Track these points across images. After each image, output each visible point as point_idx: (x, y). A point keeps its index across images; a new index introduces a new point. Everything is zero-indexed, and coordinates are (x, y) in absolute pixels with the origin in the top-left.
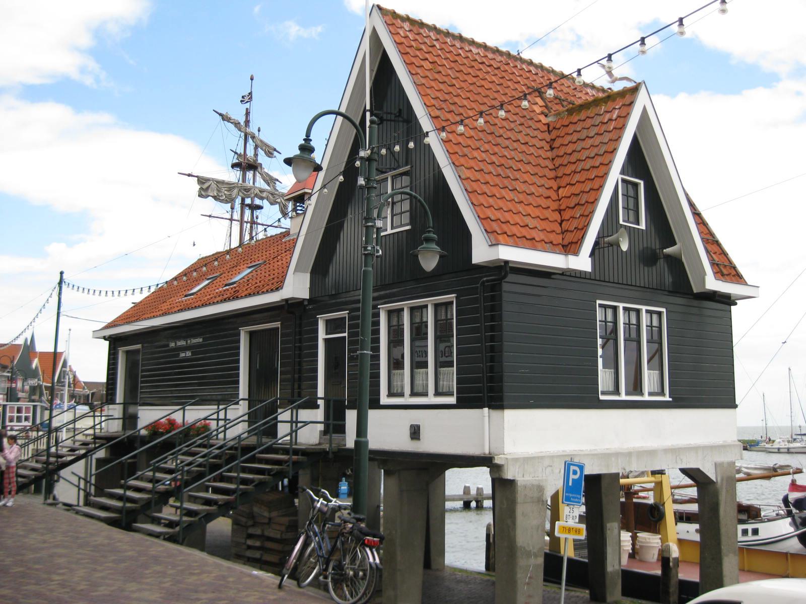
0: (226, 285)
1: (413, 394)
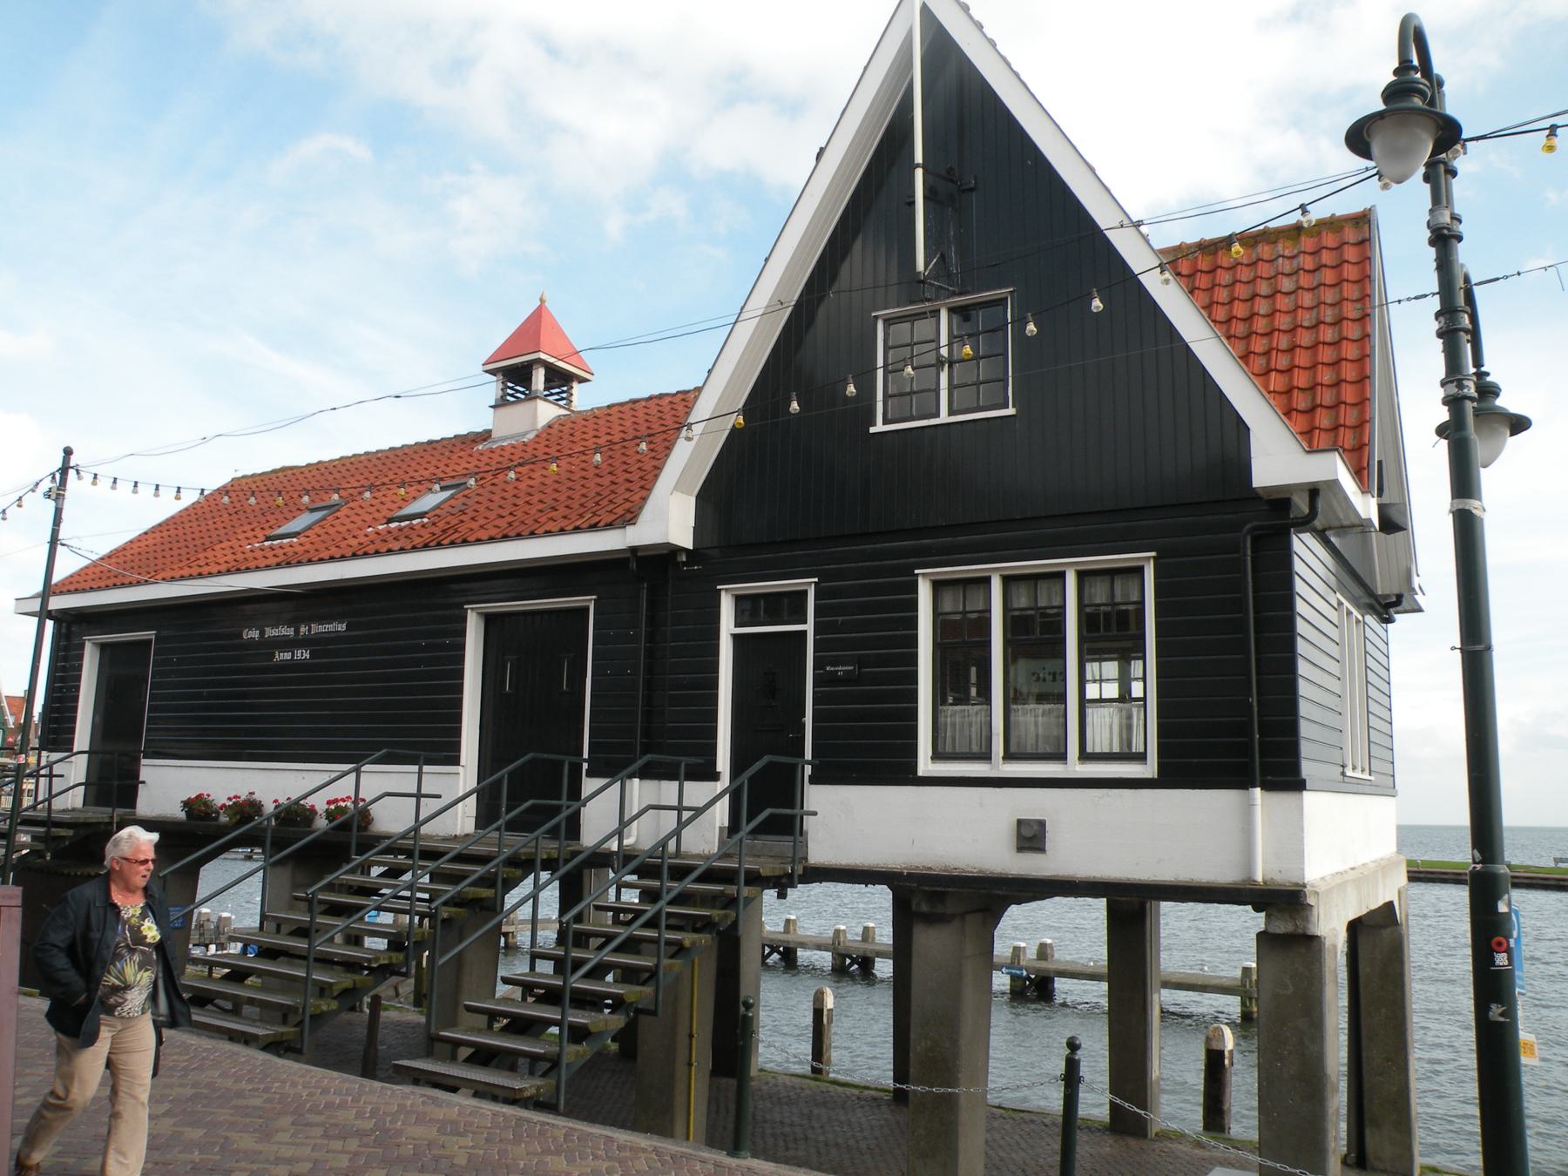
0: (268, 539)
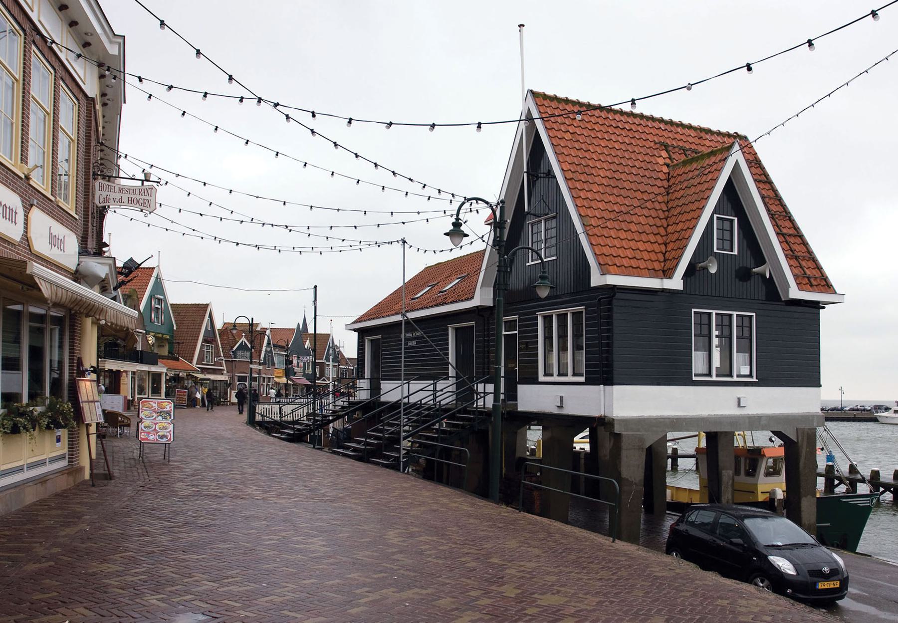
0: (440, 292)
1: (560, 375)
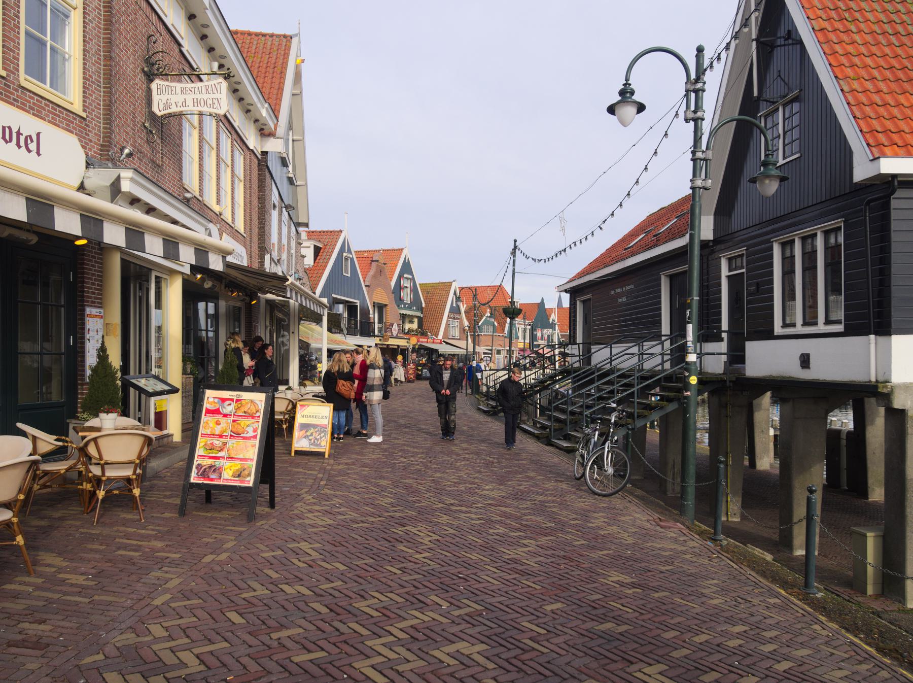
1: (805, 324)
